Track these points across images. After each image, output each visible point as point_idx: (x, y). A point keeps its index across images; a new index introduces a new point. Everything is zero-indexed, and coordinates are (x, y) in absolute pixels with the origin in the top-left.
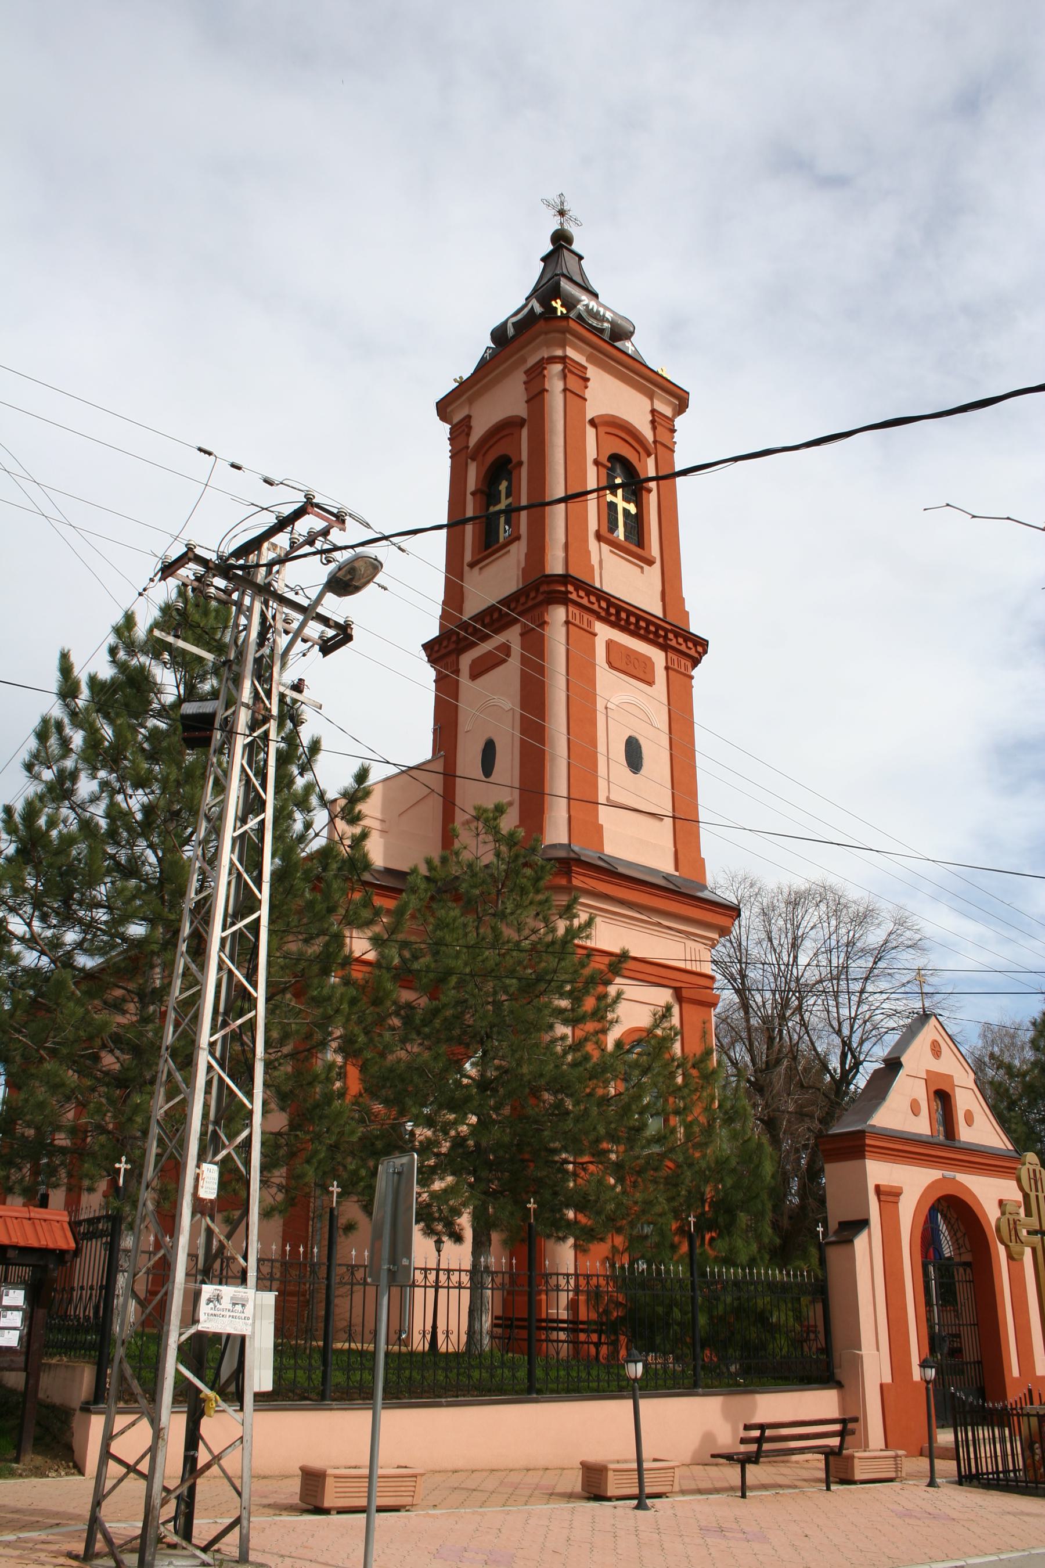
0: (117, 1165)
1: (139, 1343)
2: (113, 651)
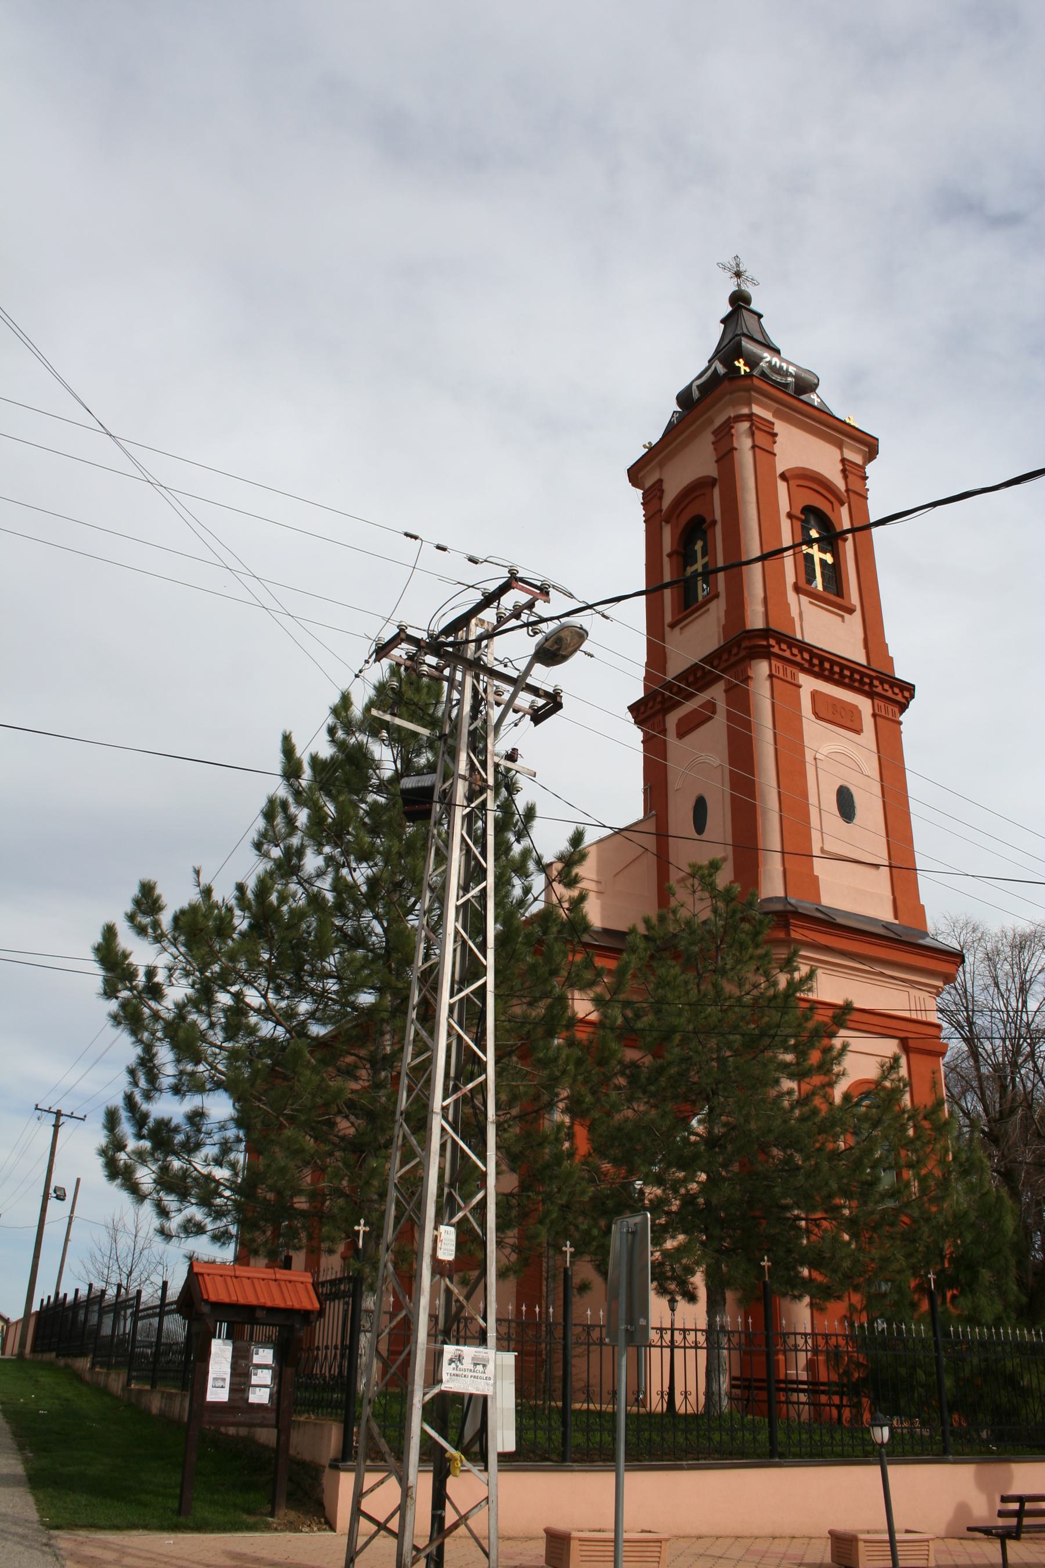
0: (356, 1228)
1: (383, 1402)
2: (332, 731)
